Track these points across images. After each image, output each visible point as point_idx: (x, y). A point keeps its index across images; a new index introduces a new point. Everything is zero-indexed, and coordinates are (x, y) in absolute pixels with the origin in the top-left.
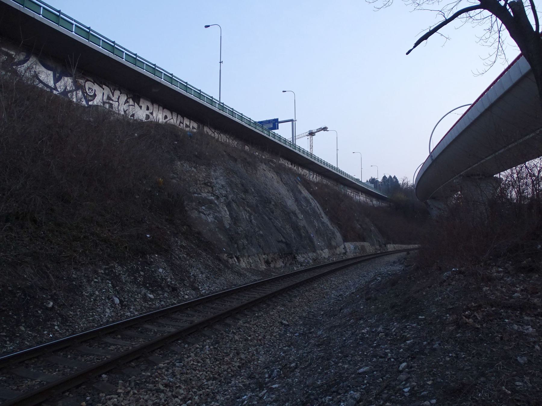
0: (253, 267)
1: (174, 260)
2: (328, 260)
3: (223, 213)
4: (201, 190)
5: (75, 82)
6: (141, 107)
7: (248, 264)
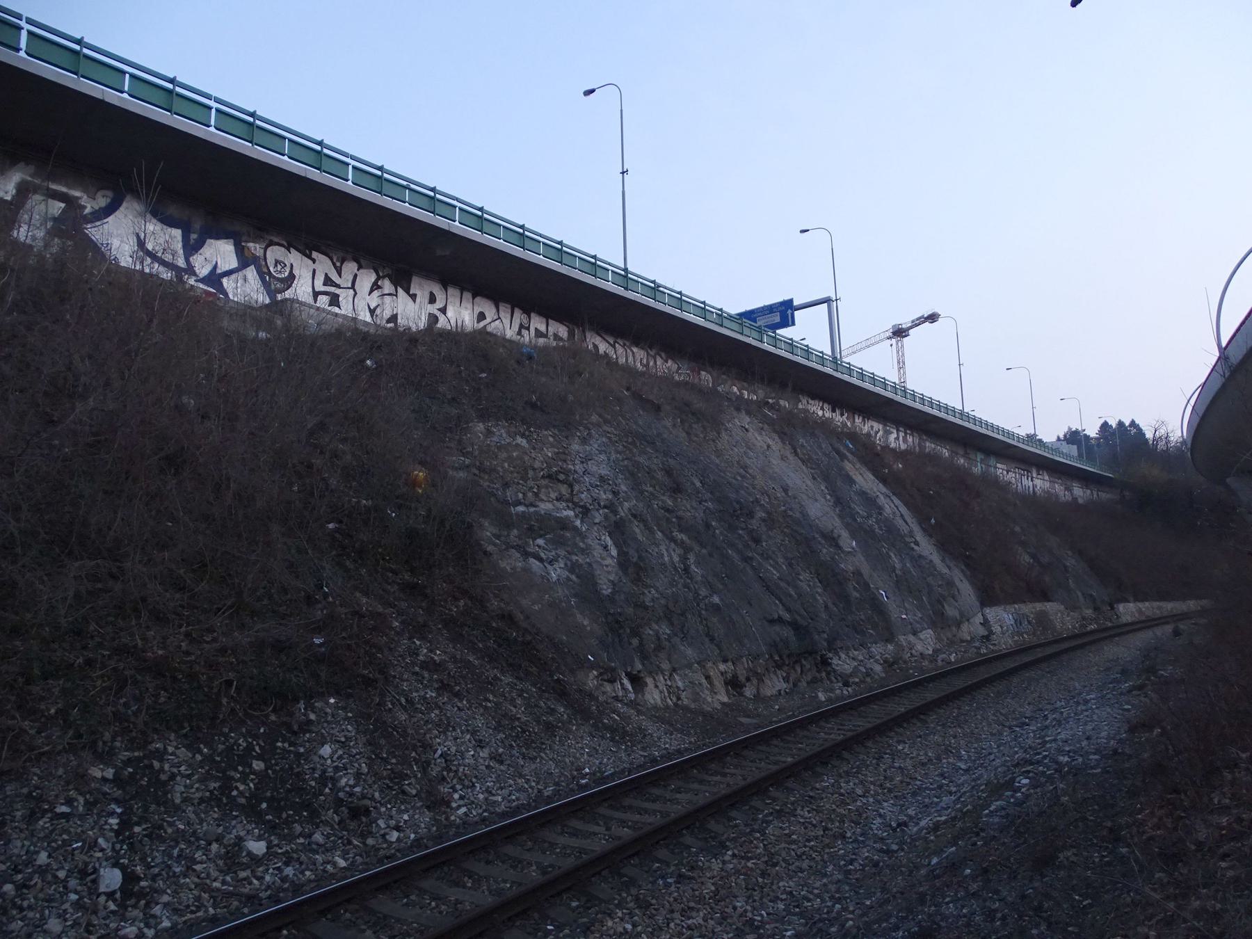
0: (686, 702)
1: (390, 709)
2: (931, 662)
3: (598, 552)
4: (536, 495)
5: (240, 251)
6: (413, 297)
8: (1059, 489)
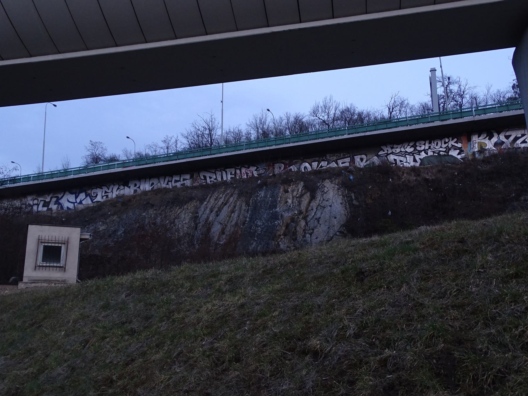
6: (129, 187)
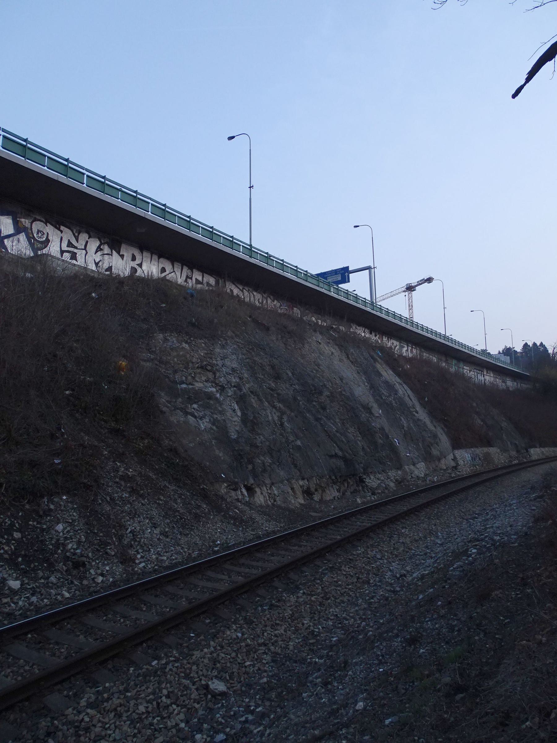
0: (279, 503)
2: (423, 481)
3: (229, 413)
4: (193, 378)
5: (16, 223)
6: (122, 256)
7: (269, 497)
8: (499, 381)
